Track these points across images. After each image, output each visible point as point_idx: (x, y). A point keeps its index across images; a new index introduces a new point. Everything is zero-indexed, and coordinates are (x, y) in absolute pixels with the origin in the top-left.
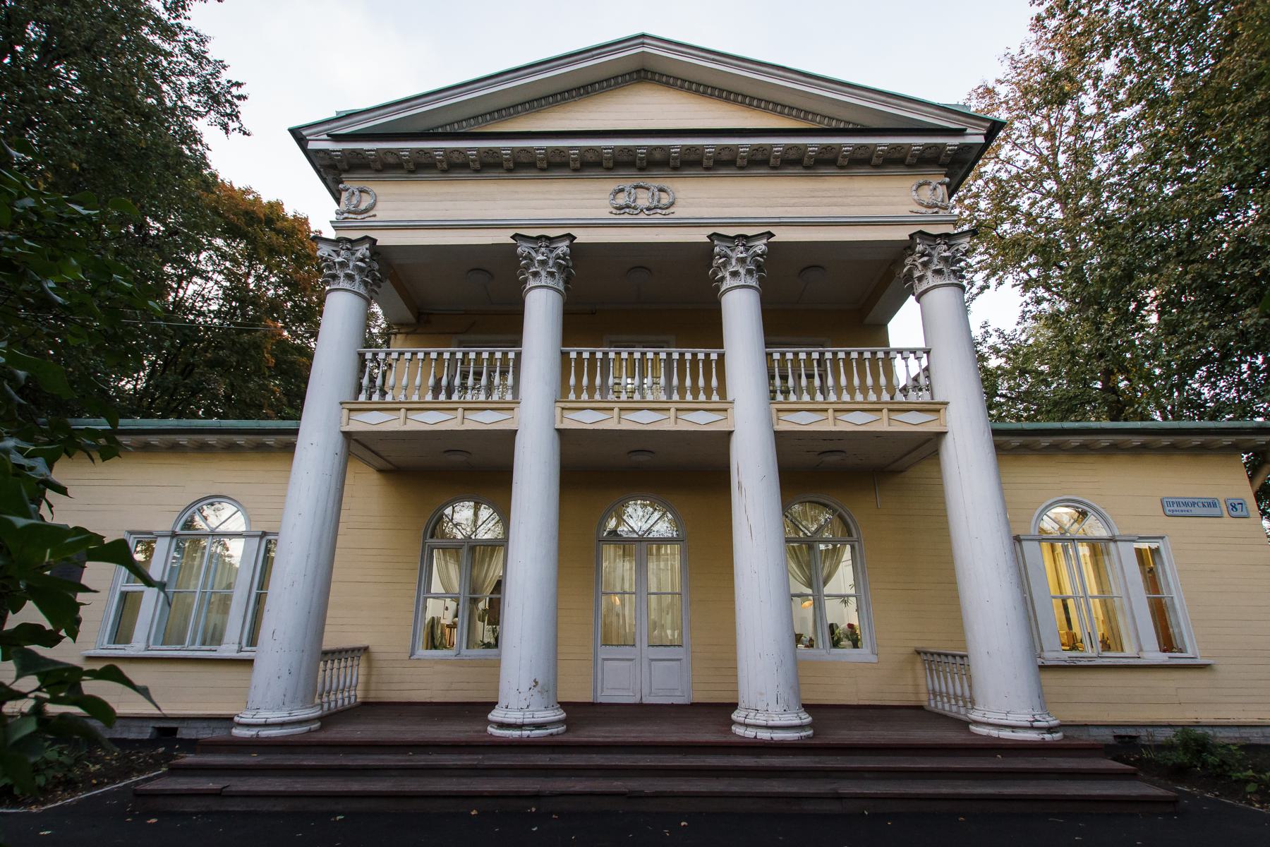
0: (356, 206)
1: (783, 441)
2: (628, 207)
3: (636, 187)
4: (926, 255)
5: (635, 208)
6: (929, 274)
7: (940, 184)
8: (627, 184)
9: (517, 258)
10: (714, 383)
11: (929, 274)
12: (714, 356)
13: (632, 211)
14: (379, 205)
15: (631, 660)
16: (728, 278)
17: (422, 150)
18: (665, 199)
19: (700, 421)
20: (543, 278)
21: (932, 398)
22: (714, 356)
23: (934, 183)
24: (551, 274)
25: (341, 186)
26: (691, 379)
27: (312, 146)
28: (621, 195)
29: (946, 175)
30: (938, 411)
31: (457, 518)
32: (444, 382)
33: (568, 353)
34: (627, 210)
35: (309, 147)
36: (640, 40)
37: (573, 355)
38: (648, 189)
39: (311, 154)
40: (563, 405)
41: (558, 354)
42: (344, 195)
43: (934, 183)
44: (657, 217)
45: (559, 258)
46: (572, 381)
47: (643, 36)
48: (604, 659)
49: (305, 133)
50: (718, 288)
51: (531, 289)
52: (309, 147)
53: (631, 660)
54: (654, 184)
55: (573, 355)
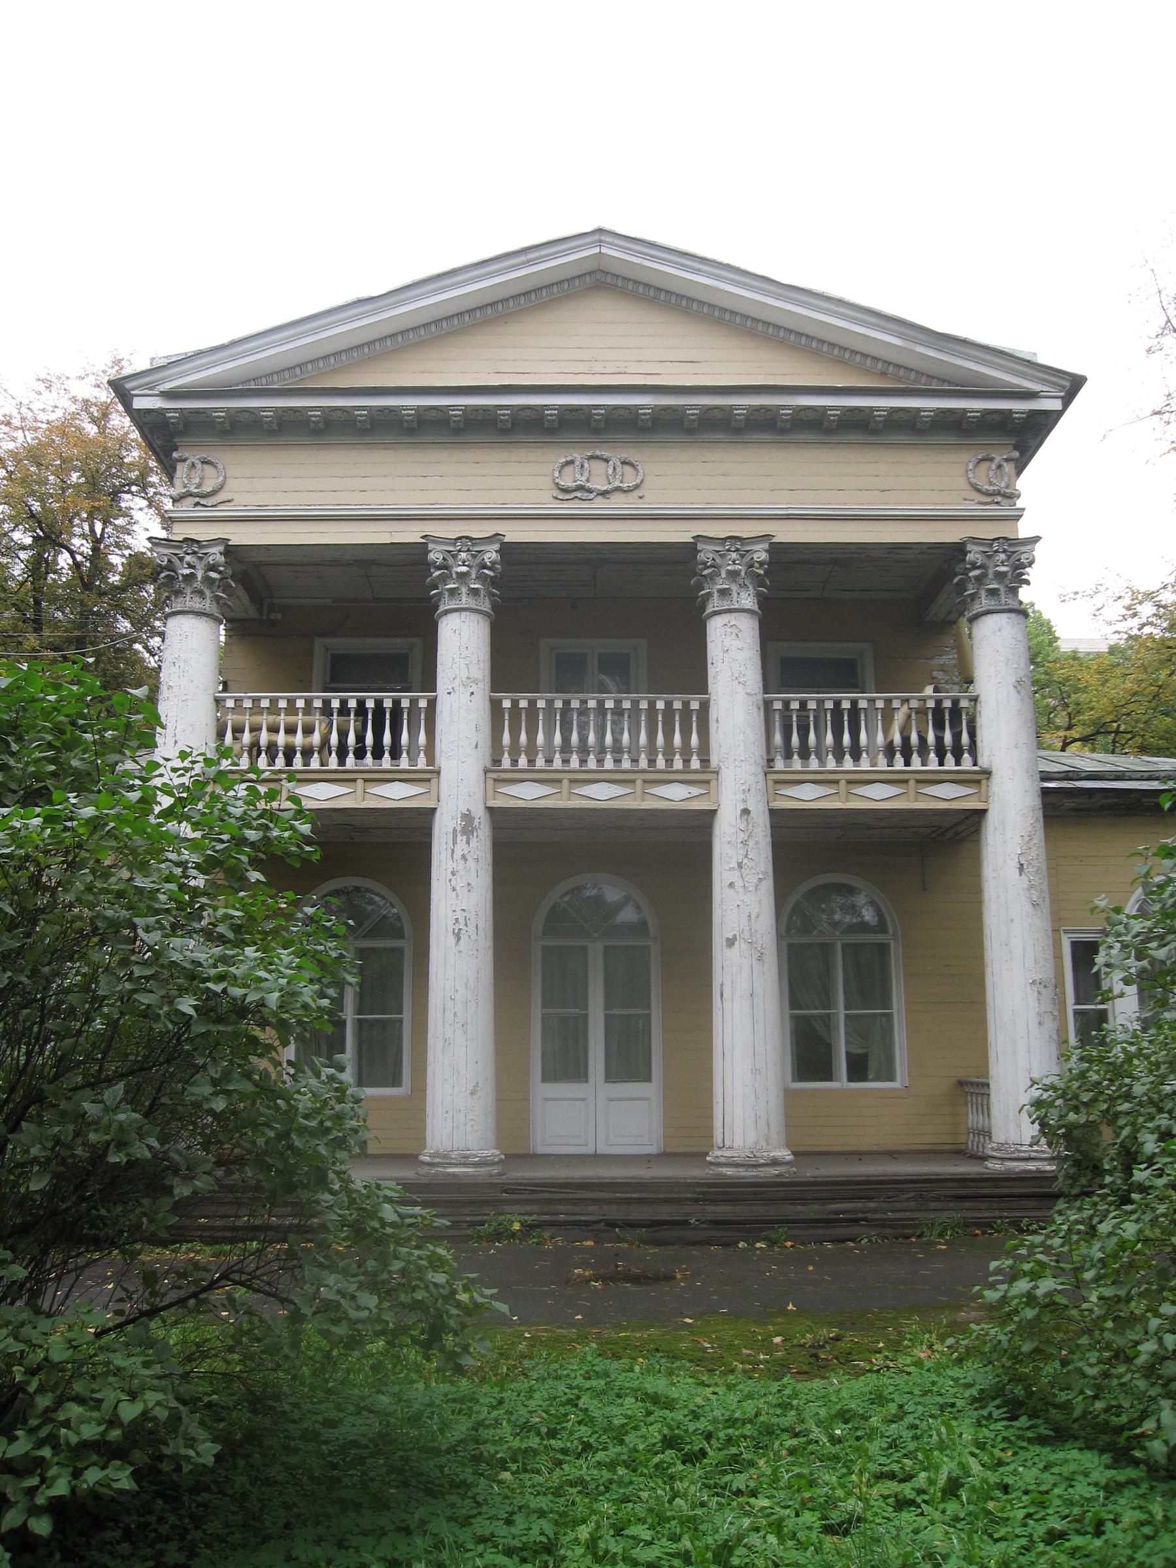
0: (199, 486)
1: (782, 822)
2: (581, 488)
3: (590, 458)
4: (979, 568)
5: (590, 491)
6: (983, 593)
7: (1007, 460)
8: (577, 456)
9: (427, 566)
10: (694, 740)
11: (983, 593)
12: (695, 705)
13: (585, 495)
14: (231, 484)
15: (583, 1100)
16: (716, 595)
17: (290, 409)
18: (630, 481)
19: (675, 796)
20: (464, 599)
21: (975, 764)
22: (695, 705)
23: (998, 459)
24: (474, 592)
25: (175, 455)
26: (426, 732)
27: (139, 404)
28: (568, 470)
29: (1016, 448)
30: (978, 782)
31: (744, 595)
32: (351, 739)
33: (500, 702)
34: (578, 494)
35: (135, 407)
36: (597, 237)
37: (507, 704)
38: (607, 461)
39: (134, 413)
40: (495, 775)
41: (487, 703)
42: (181, 469)
43: (998, 459)
44: (618, 504)
45: (485, 567)
46: (506, 738)
47: (600, 231)
48: (547, 1099)
49: (128, 386)
50: (703, 608)
51: (447, 612)
52: (135, 407)
53: (583, 1100)
54: (616, 455)
55: (507, 704)
